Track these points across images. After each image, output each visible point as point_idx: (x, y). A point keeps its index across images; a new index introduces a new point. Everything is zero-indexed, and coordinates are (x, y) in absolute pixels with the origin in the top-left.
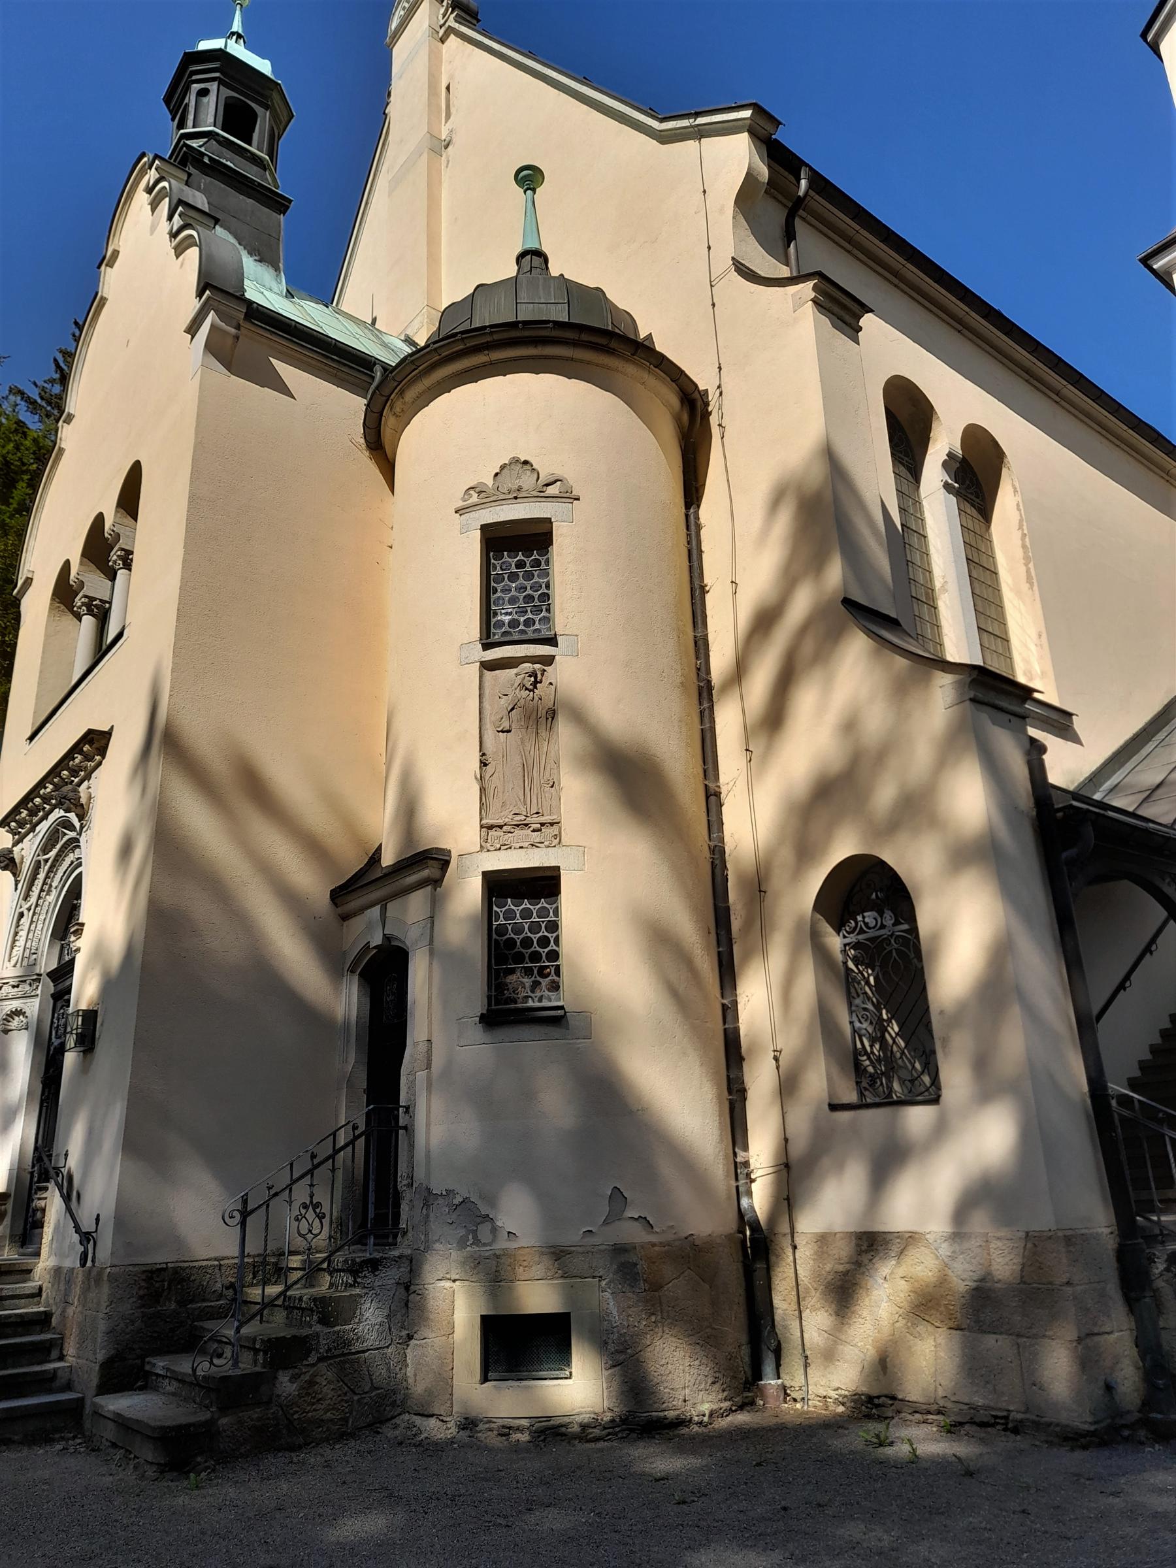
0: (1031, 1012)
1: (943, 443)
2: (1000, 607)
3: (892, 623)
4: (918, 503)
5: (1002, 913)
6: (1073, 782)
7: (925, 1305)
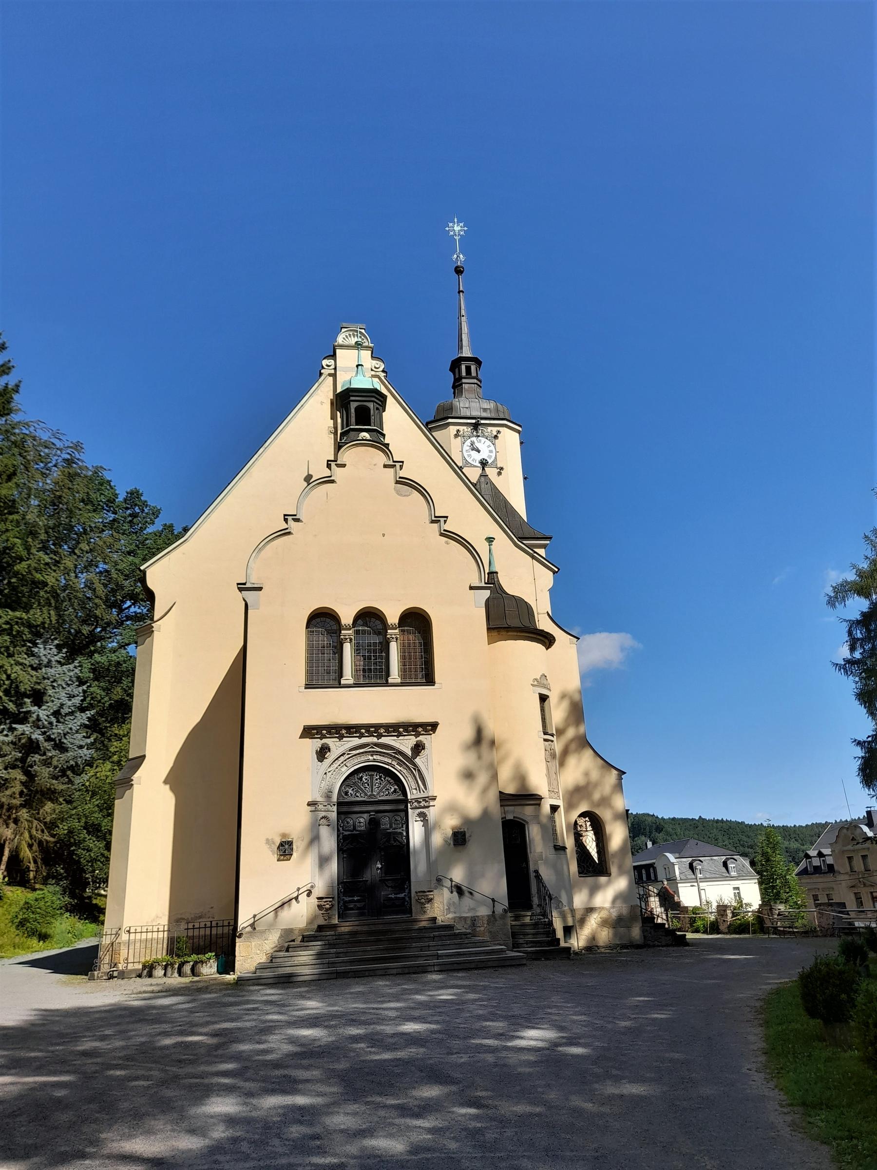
7: (604, 923)
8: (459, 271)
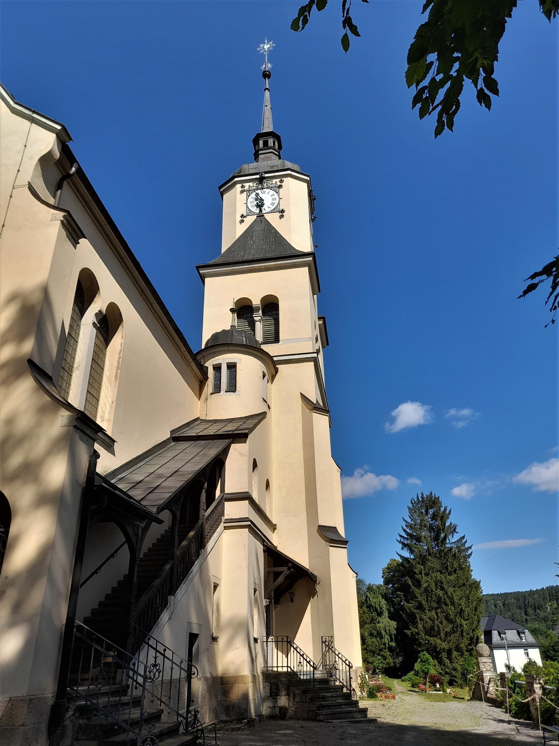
0: (52, 582)
1: (98, 305)
2: (100, 384)
3: (49, 378)
4: (79, 326)
5: (54, 531)
6: (105, 472)
8: (266, 75)
